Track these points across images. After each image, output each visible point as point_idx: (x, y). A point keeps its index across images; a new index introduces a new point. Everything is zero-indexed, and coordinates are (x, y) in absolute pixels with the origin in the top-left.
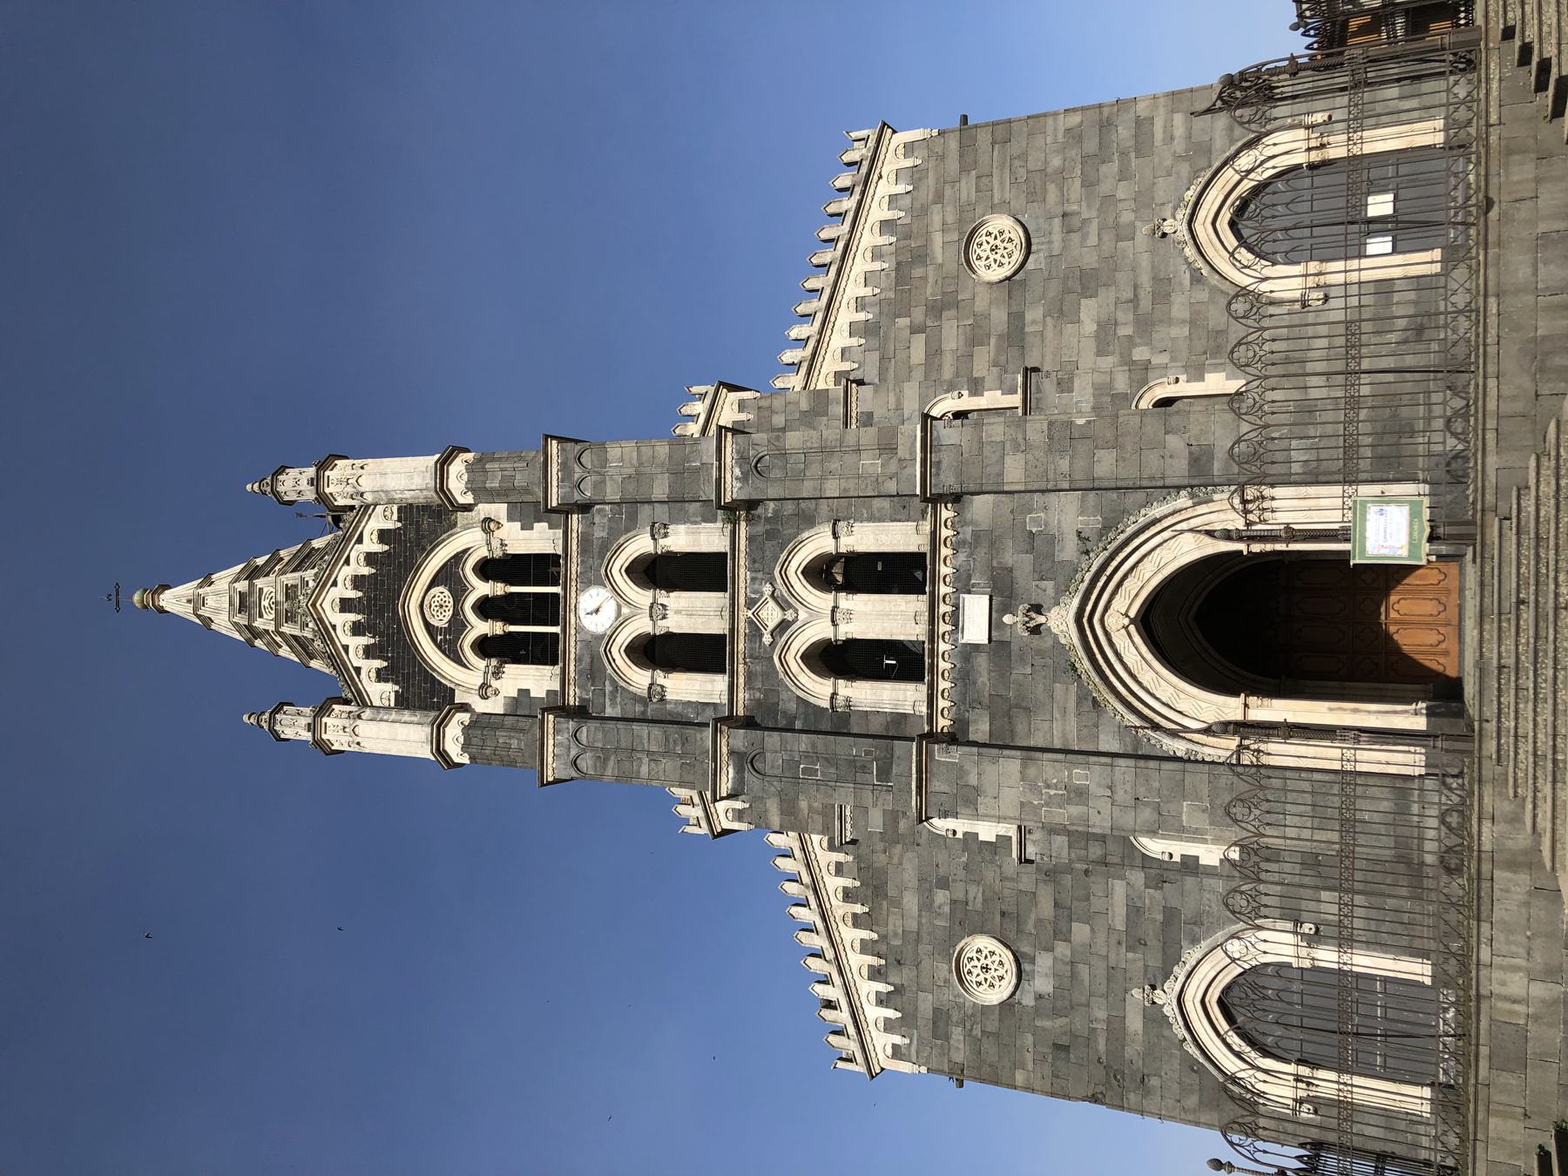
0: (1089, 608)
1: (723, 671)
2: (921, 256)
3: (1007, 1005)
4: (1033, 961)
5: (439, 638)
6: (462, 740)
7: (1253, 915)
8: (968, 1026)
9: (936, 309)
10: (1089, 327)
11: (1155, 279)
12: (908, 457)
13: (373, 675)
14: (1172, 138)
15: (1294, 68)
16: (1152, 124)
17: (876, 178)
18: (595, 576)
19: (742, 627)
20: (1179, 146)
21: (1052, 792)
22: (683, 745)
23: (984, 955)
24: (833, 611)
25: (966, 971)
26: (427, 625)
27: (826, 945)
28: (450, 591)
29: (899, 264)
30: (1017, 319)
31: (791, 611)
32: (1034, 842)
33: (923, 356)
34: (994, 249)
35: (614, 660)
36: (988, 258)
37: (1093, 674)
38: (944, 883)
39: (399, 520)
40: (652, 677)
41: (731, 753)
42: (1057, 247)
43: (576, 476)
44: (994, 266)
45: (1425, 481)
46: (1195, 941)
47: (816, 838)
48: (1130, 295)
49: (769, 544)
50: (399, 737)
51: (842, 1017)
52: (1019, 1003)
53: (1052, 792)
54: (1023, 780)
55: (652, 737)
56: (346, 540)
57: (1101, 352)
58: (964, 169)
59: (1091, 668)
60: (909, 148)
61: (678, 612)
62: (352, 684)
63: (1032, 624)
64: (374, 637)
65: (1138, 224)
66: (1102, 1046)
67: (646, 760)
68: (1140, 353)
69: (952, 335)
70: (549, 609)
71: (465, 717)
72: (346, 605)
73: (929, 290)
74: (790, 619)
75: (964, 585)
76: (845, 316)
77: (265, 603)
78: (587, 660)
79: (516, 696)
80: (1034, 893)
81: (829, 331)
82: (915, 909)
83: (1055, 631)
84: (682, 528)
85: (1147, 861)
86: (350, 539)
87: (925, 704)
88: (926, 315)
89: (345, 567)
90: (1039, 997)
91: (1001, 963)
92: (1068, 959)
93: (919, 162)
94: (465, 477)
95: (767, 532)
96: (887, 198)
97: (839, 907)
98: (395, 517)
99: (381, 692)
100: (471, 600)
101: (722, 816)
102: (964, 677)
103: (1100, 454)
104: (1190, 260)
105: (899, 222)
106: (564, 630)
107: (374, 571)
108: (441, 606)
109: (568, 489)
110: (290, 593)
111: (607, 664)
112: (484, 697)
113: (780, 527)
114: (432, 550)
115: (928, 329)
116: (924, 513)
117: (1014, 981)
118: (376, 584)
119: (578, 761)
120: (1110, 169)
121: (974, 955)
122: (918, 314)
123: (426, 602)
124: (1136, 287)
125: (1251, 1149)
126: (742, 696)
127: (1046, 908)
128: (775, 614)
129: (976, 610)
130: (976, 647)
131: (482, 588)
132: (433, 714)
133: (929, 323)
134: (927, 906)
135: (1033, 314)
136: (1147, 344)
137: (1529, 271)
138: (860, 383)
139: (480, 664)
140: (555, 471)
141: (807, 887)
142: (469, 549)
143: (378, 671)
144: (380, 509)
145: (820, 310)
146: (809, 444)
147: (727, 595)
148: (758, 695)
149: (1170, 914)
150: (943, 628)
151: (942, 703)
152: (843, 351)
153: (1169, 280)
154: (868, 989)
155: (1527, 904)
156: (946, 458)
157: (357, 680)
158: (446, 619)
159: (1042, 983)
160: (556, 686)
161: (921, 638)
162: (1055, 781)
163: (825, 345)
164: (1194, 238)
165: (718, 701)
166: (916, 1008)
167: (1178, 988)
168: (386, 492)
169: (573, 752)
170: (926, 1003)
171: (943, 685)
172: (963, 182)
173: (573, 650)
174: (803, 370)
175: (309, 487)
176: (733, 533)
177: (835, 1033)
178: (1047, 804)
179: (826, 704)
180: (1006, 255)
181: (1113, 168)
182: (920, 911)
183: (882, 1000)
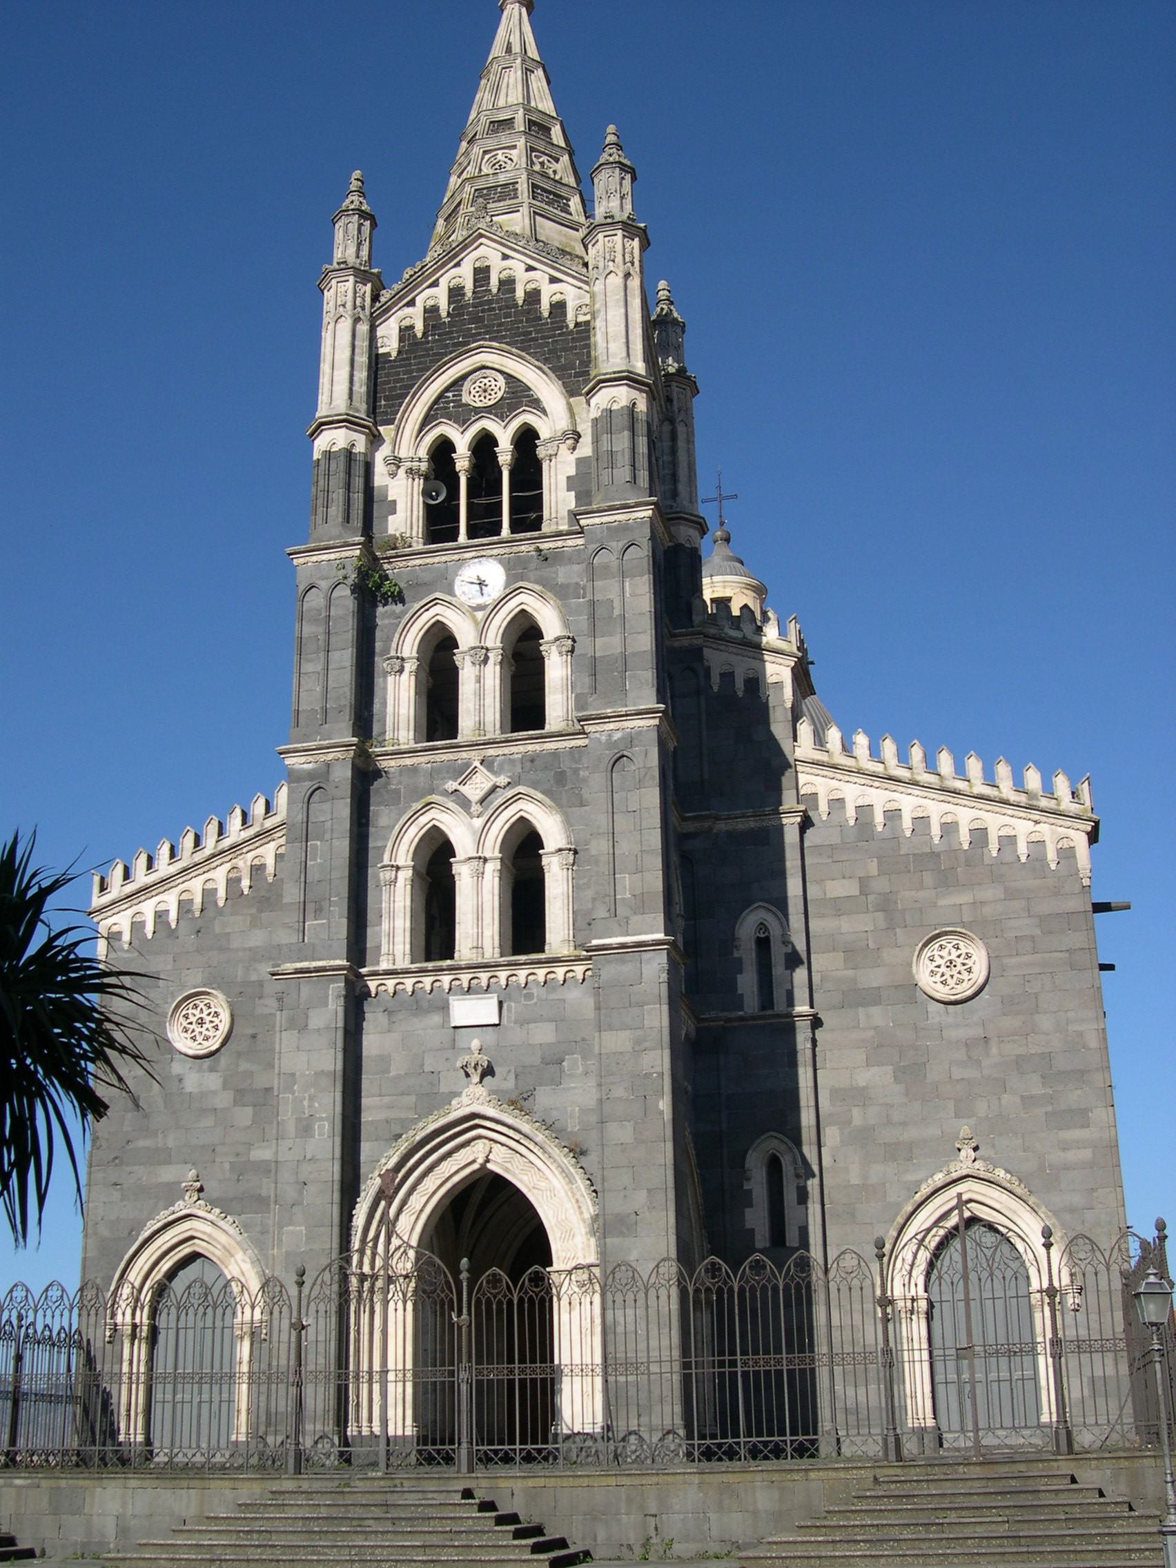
2: (947, 880)
3: (171, 1050)
5: (450, 394)
9: (886, 905)
10: (863, 1077)
14: (1064, 1150)
16: (1082, 1127)
17: (1037, 818)
18: (517, 573)
20: (1056, 1157)
23: (214, 1019)
25: (184, 1013)
26: (464, 377)
27: (208, 852)
29: (938, 855)
30: (872, 997)
35: (427, 610)
39: (577, 324)
40: (410, 658)
41: (328, 765)
42: (952, 1034)
51: (141, 877)
53: (306, 1103)
60: (1067, 854)
62: (396, 299)
63: (470, 1070)
64: (449, 314)
65: (972, 1121)
66: (142, 1143)
70: (484, 525)
71: (361, 446)
72: (482, 274)
74: (473, 809)
76: (879, 798)
81: (863, 781)
82: (252, 944)
87: (391, 967)
88: (879, 894)
89: (523, 267)
95: (563, 773)
98: (581, 319)
103: (629, 1126)
107: (520, 302)
108: (485, 391)
111: (422, 603)
115: (864, 897)
117: (191, 1052)
119: (314, 589)
120: (1036, 1088)
121: (213, 1010)
122: (881, 885)
123: (488, 372)
124: (904, 1124)
125: (45, 1307)
128: (478, 791)
129: (480, 1010)
130: (445, 1008)
131: (505, 438)
134: (255, 956)
135: (877, 1016)
136: (842, 1141)
139: (423, 453)
142: (544, 412)
145: (885, 768)
150: (465, 978)
151: (390, 983)
152: (841, 801)
154: (170, 901)
162: (316, 1105)
166: (157, 953)
167: (201, 1213)
173: (437, 560)
177: (172, 849)
180: (944, 978)
181: (1038, 1089)
182: (250, 949)
183: (160, 916)
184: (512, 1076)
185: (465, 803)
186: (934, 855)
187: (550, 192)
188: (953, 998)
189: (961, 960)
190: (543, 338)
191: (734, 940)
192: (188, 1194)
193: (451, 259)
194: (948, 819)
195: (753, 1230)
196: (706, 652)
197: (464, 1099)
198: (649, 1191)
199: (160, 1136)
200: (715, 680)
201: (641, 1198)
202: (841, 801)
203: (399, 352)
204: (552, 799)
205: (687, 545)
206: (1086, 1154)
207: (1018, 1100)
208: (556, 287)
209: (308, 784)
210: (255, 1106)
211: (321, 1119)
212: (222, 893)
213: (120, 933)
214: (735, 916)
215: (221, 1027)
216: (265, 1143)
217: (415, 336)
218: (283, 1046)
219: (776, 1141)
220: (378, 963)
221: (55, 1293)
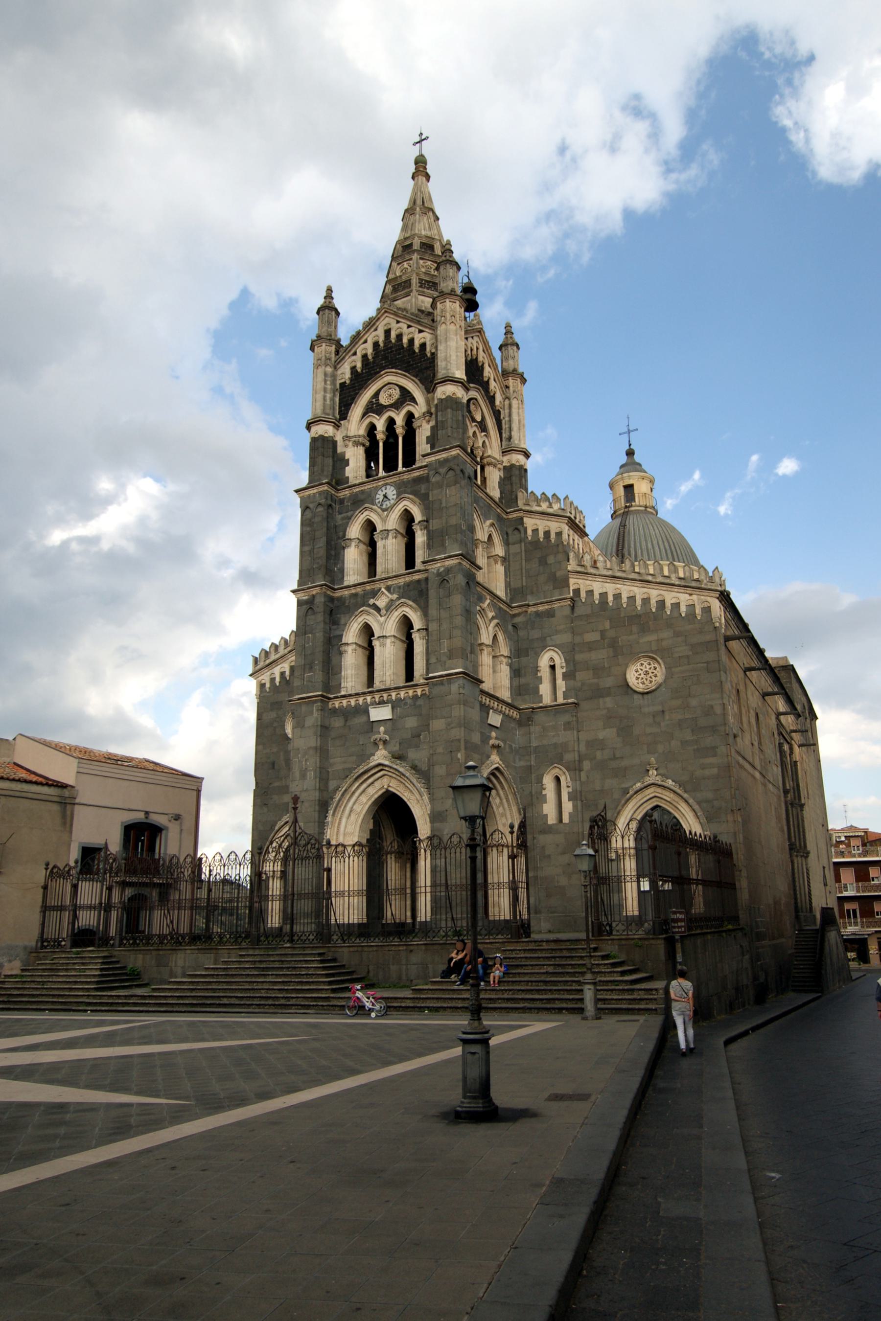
2: (644, 629)
9: (613, 644)
10: (601, 735)
12: (447, 666)
14: (703, 769)
17: (690, 592)
24: (383, 637)
29: (640, 616)
33: (589, 640)
34: (647, 673)
41: (314, 596)
42: (646, 710)
48: (617, 756)
60: (707, 610)
65: (656, 755)
68: (587, 765)
69: (599, 656)
75: (395, 705)
76: (610, 588)
86: (420, 325)
89: (406, 326)
99: (345, 373)
103: (444, 767)
107: (405, 346)
120: (688, 736)
122: (611, 634)
123: (391, 386)
130: (367, 713)
131: (400, 419)
133: (606, 641)
135: (608, 702)
138: (573, 608)
139: (362, 431)
142: (417, 404)
148: (347, 602)
150: (377, 697)
151: (345, 702)
169: (311, 506)
174: (579, 569)
179: (343, 641)
183: (282, 674)
184: (398, 745)
185: (378, 609)
186: (639, 616)
187: (430, 282)
188: (646, 691)
189: (651, 671)
190: (416, 364)
191: (537, 667)
195: (547, 815)
196: (525, 519)
197: (376, 757)
199: (284, 780)
200: (529, 532)
204: (417, 604)
205: (517, 464)
206: (715, 771)
208: (422, 335)
213: (265, 684)
214: (537, 655)
219: (557, 769)
221: (233, 857)
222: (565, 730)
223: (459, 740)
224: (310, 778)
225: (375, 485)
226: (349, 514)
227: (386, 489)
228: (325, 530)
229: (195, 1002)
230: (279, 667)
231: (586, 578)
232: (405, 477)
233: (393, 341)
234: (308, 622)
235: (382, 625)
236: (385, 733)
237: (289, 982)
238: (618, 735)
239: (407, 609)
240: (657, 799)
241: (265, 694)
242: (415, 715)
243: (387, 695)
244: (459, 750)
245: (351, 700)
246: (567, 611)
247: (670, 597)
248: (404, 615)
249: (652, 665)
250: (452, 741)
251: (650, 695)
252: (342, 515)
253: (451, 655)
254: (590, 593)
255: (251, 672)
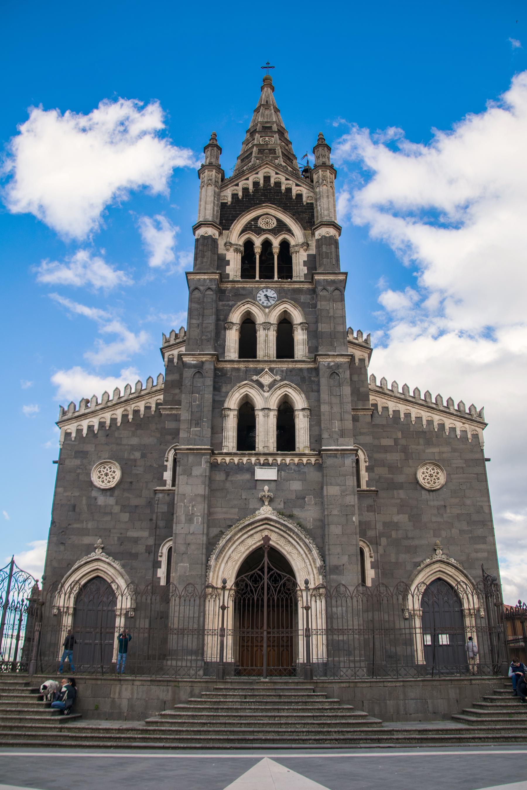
0: (272, 523)
1: (240, 357)
2: (429, 443)
3: (91, 484)
4: (111, 496)
6: (206, 235)
7: (136, 593)
8: (81, 467)
10: (396, 519)
11: (416, 547)
13: (235, 192)
14: (477, 552)
15: (499, 604)
16: (483, 543)
17: (464, 421)
19: (260, 366)
20: (474, 555)
21: (190, 508)
22: (206, 339)
28: (275, 227)
29: (425, 432)
30: (400, 486)
31: (268, 389)
32: (164, 496)
33: (384, 444)
34: (431, 476)
36: (427, 473)
37: (243, 525)
38: (143, 456)
39: (307, 204)
41: (203, 362)
42: (431, 503)
43: (329, 288)
44: (423, 476)
45: (328, 660)
46: (123, 566)
47: (162, 397)
49: (299, 378)
50: (207, 206)
52: (92, 490)
53: (190, 508)
54: (195, 495)
55: (209, 325)
56: (298, 178)
57: (385, 524)
58: (466, 461)
59: (245, 524)
61: (267, 336)
65: (440, 539)
67: (198, 322)
68: (384, 541)
69: (394, 457)
70: (266, 274)
72: (267, 179)
73: (413, 446)
74: (264, 389)
75: (282, 468)
77: (267, 139)
78: (244, 292)
79: (227, 259)
80: (141, 497)
82: (132, 443)
83: (261, 509)
84: (305, 337)
85: (157, 546)
86: (298, 180)
87: (227, 451)
90: (96, 499)
91: (109, 482)
92: (112, 511)
93: (470, 441)
94: (327, 235)
95: (304, 377)
96: (454, 427)
97: (131, 408)
98: (309, 201)
99: (228, 195)
100: (270, 237)
101: (170, 353)
102: (240, 468)
103: (340, 527)
104: (424, 562)
105: (444, 432)
106: (257, 282)
107: (283, 192)
108: (267, 223)
109: (323, 284)
110: (273, 151)
112: (225, 244)
113: (307, 383)
114: (294, 219)
116: (314, 450)
117: (102, 487)
118: (278, 193)
119: (197, 290)
121: (113, 470)
122: (403, 442)
123: (269, 216)
124: (413, 538)
126: (228, 366)
127: (135, 501)
128: (267, 382)
129: (271, 474)
130: (253, 473)
131: (276, 242)
132: (218, 221)
133: (399, 447)
134: (133, 448)
135: (402, 494)
137: (413, 697)
139: (241, 242)
140: (330, 277)
141: (140, 393)
142: (293, 234)
143: (237, 194)
144: (312, 194)
146: (345, 397)
147: (275, 359)
148: (229, 374)
149: (135, 556)
151: (228, 459)
153: (416, 553)
155: (158, 699)
156: (338, 461)
157: (233, 184)
158: (261, 226)
159: (101, 500)
160: (231, 279)
161: (257, 449)
163: (389, 399)
164: (434, 563)
165: (226, 355)
167: (103, 559)
168: (320, 198)
169: (201, 288)
170: (90, 448)
171: (236, 460)
172: (461, 461)
175: (321, 163)
176: (303, 361)
178: (185, 506)
179: (226, 405)
181: (465, 527)
182: (131, 445)
186: (424, 432)
192: (97, 550)
193: (254, 170)
194: (430, 419)
198: (349, 556)
199: (85, 523)
201: (345, 559)
202: (387, 408)
203: (232, 203)
207: (458, 532)
208: (298, 188)
209: (193, 370)
210: (130, 513)
211: (197, 516)
212: (119, 420)
215: (116, 477)
216: (134, 530)
217: (238, 198)
218: (180, 482)
220: (221, 450)
222: (368, 511)
223: (354, 506)
224: (197, 523)
225: (256, 286)
226: (231, 303)
227: (267, 291)
228: (214, 310)
229: (232, 737)
230: (87, 421)
231: (383, 397)
232: (286, 286)
233: (272, 185)
234: (195, 383)
235: (266, 400)
236: (269, 491)
237: (320, 716)
238: (410, 520)
239: (290, 390)
240: (440, 573)
241: (69, 442)
242: (299, 480)
243: (306, 459)
244: (353, 514)
245: (235, 458)
246: (369, 419)
247: (449, 423)
248: (247, 394)
249: (436, 471)
250: (347, 506)
251: (434, 492)
252: (224, 303)
253: (342, 433)
254: (386, 409)
255: (57, 420)
